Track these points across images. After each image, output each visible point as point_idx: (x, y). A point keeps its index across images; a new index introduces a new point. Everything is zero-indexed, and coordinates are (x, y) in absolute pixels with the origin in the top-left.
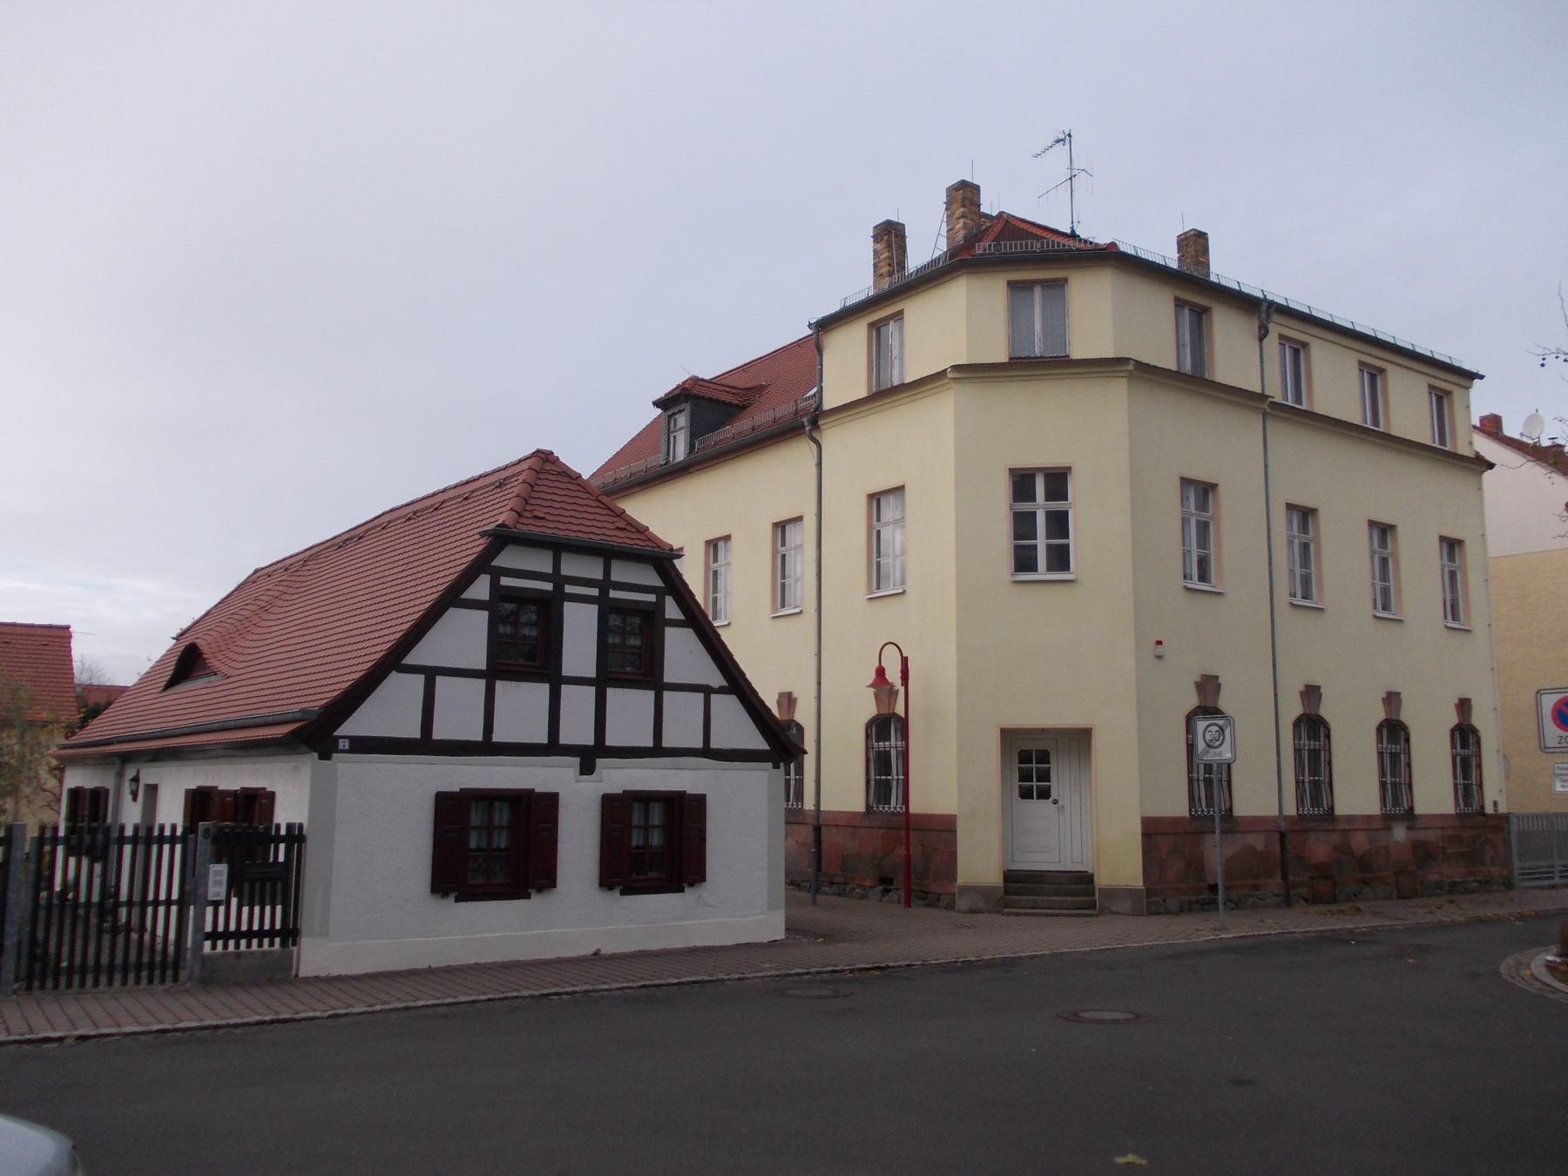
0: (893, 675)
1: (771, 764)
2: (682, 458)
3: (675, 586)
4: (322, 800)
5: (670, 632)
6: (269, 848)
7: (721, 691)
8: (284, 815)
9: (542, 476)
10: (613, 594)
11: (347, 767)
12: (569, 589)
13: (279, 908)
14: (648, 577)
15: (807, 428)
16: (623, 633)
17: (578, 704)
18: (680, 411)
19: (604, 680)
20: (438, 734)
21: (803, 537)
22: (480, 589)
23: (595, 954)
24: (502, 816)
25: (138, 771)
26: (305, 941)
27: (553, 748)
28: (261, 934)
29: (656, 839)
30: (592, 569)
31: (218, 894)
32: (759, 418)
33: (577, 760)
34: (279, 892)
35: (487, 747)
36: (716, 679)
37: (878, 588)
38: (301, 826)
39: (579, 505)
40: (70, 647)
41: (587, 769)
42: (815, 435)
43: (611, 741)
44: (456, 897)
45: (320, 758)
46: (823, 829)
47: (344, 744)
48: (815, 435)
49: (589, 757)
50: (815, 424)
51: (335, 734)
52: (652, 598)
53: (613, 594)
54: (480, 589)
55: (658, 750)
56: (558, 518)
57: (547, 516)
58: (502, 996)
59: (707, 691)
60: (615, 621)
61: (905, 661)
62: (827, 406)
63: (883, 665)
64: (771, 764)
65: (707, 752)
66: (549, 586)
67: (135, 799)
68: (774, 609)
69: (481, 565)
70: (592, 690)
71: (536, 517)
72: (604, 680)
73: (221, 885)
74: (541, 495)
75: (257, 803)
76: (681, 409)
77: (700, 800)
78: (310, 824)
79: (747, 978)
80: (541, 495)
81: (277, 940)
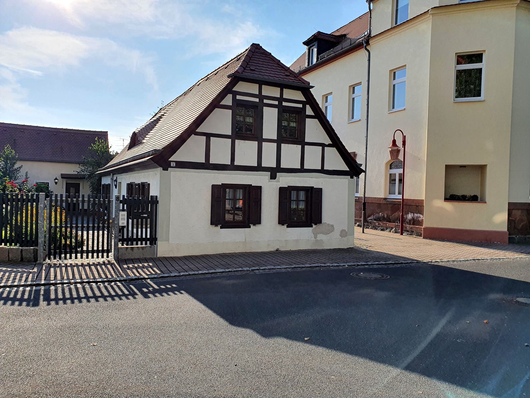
0: (399, 143)
1: (349, 177)
2: (315, 63)
3: (311, 100)
4: (165, 185)
5: (308, 120)
6: (149, 205)
7: (329, 145)
8: (154, 192)
9: (254, 54)
10: (284, 104)
11: (175, 174)
12: (265, 101)
13: (106, 232)
14: (298, 96)
15: (364, 45)
16: (289, 121)
17: (269, 149)
18: (313, 46)
19: (280, 141)
20: (212, 161)
21: (361, 91)
22: (228, 100)
23: (277, 250)
24: (240, 194)
25: (117, 177)
26: (159, 243)
27: (259, 168)
28: (142, 240)
29: (302, 206)
30: (275, 92)
31: (123, 223)
32: (345, 45)
33: (269, 173)
34: (144, 223)
35: (233, 167)
36: (327, 141)
37: (393, 108)
38: (156, 197)
39: (266, 60)
40: (108, 138)
41: (273, 177)
42: (368, 48)
43: (283, 166)
44: (220, 226)
45: (163, 170)
46: (366, 204)
47: (173, 164)
48: (368, 48)
49: (274, 172)
50: (368, 43)
51: (169, 160)
52: (300, 106)
53: (284, 104)
54: (228, 100)
55: (302, 170)
56: (261, 70)
57: (256, 70)
58: (235, 270)
59: (323, 145)
60: (286, 115)
61: (404, 137)
62: (372, 35)
63: (395, 139)
64: (349, 177)
65: (322, 171)
66: (257, 100)
67: (116, 188)
68: (349, 120)
69: (227, 90)
70: (275, 145)
71: (251, 70)
72: (280, 141)
73: (125, 220)
74: (254, 61)
75: (144, 187)
76: (314, 44)
77: (320, 190)
78: (160, 195)
79: (340, 266)
80: (254, 61)
81: (148, 242)
